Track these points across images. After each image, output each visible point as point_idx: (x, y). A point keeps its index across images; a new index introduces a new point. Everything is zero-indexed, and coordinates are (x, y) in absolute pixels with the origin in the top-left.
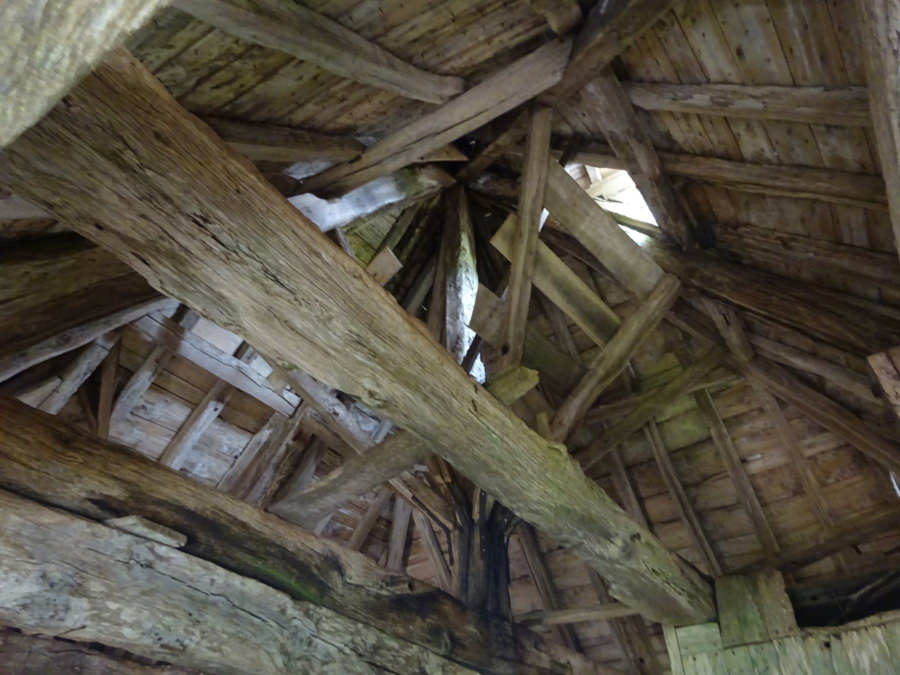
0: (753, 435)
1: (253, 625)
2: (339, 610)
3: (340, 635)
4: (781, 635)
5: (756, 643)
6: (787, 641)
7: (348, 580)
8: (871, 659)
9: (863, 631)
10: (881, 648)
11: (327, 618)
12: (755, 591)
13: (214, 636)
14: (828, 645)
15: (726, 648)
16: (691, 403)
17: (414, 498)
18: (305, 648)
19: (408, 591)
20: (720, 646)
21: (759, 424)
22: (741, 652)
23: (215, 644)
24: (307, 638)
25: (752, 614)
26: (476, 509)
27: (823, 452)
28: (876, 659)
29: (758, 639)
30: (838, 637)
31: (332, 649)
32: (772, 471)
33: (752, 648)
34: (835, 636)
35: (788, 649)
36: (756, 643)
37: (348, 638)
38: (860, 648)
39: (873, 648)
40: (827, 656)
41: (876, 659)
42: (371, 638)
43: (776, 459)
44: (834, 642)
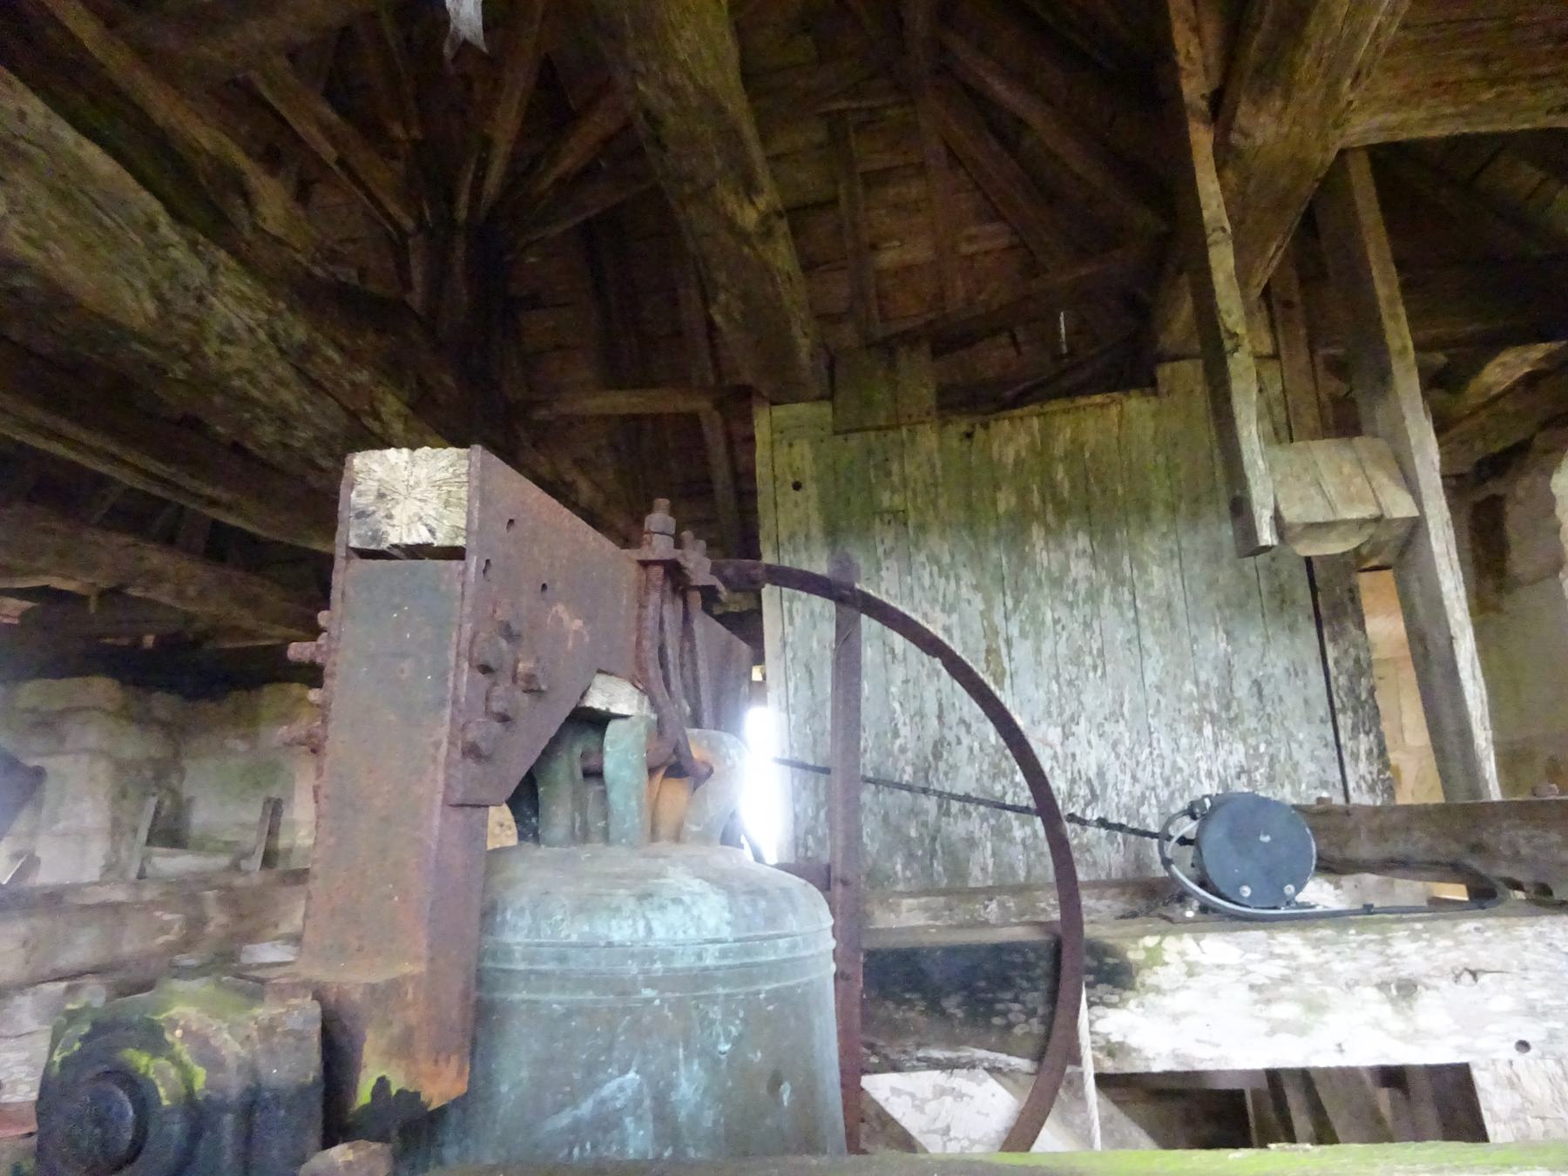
0: (897, 207)
1: (101, 225)
2: (248, 264)
3: (249, 306)
4: (914, 419)
5: (879, 429)
6: (920, 427)
7: (261, 223)
8: (1018, 453)
9: (1018, 421)
10: (1033, 442)
11: (227, 269)
12: (892, 366)
13: (32, 217)
14: (969, 435)
15: (836, 433)
16: (819, 135)
17: (341, 162)
18: (193, 303)
19: (356, 282)
20: (829, 429)
21: (914, 190)
22: (855, 440)
23: (34, 233)
24: (196, 288)
25: (881, 395)
26: (464, 198)
27: (987, 253)
28: (1023, 454)
29: (882, 423)
30: (986, 426)
31: (236, 323)
32: (908, 269)
33: (872, 434)
34: (982, 425)
35: (918, 438)
36: (879, 429)
37: (263, 316)
38: (1009, 439)
39: (1023, 440)
40: (965, 448)
41: (1023, 454)
42: (300, 333)
43: (919, 251)
44: (980, 434)
